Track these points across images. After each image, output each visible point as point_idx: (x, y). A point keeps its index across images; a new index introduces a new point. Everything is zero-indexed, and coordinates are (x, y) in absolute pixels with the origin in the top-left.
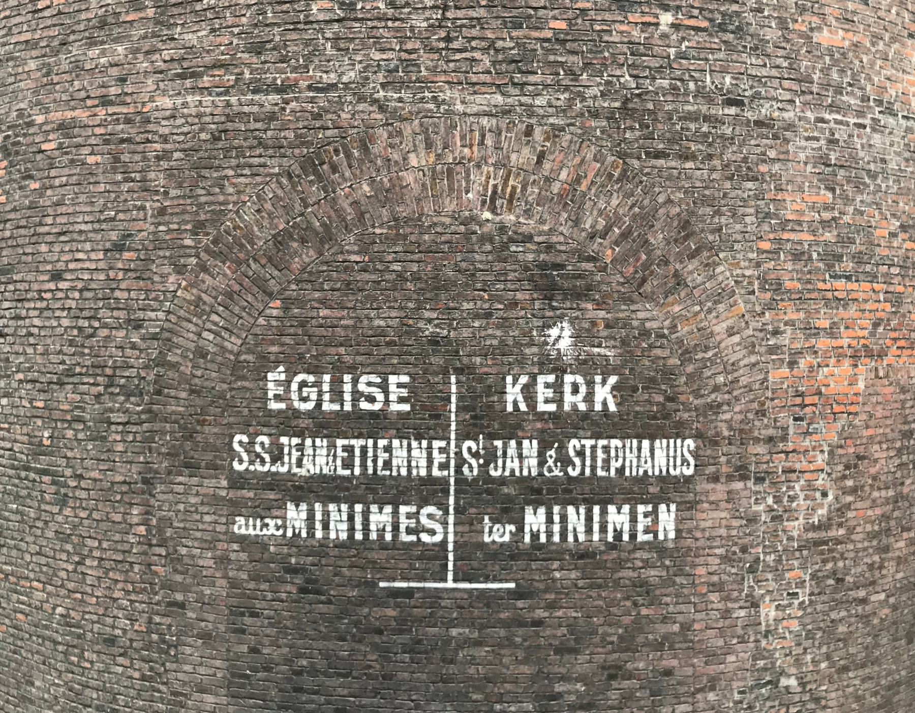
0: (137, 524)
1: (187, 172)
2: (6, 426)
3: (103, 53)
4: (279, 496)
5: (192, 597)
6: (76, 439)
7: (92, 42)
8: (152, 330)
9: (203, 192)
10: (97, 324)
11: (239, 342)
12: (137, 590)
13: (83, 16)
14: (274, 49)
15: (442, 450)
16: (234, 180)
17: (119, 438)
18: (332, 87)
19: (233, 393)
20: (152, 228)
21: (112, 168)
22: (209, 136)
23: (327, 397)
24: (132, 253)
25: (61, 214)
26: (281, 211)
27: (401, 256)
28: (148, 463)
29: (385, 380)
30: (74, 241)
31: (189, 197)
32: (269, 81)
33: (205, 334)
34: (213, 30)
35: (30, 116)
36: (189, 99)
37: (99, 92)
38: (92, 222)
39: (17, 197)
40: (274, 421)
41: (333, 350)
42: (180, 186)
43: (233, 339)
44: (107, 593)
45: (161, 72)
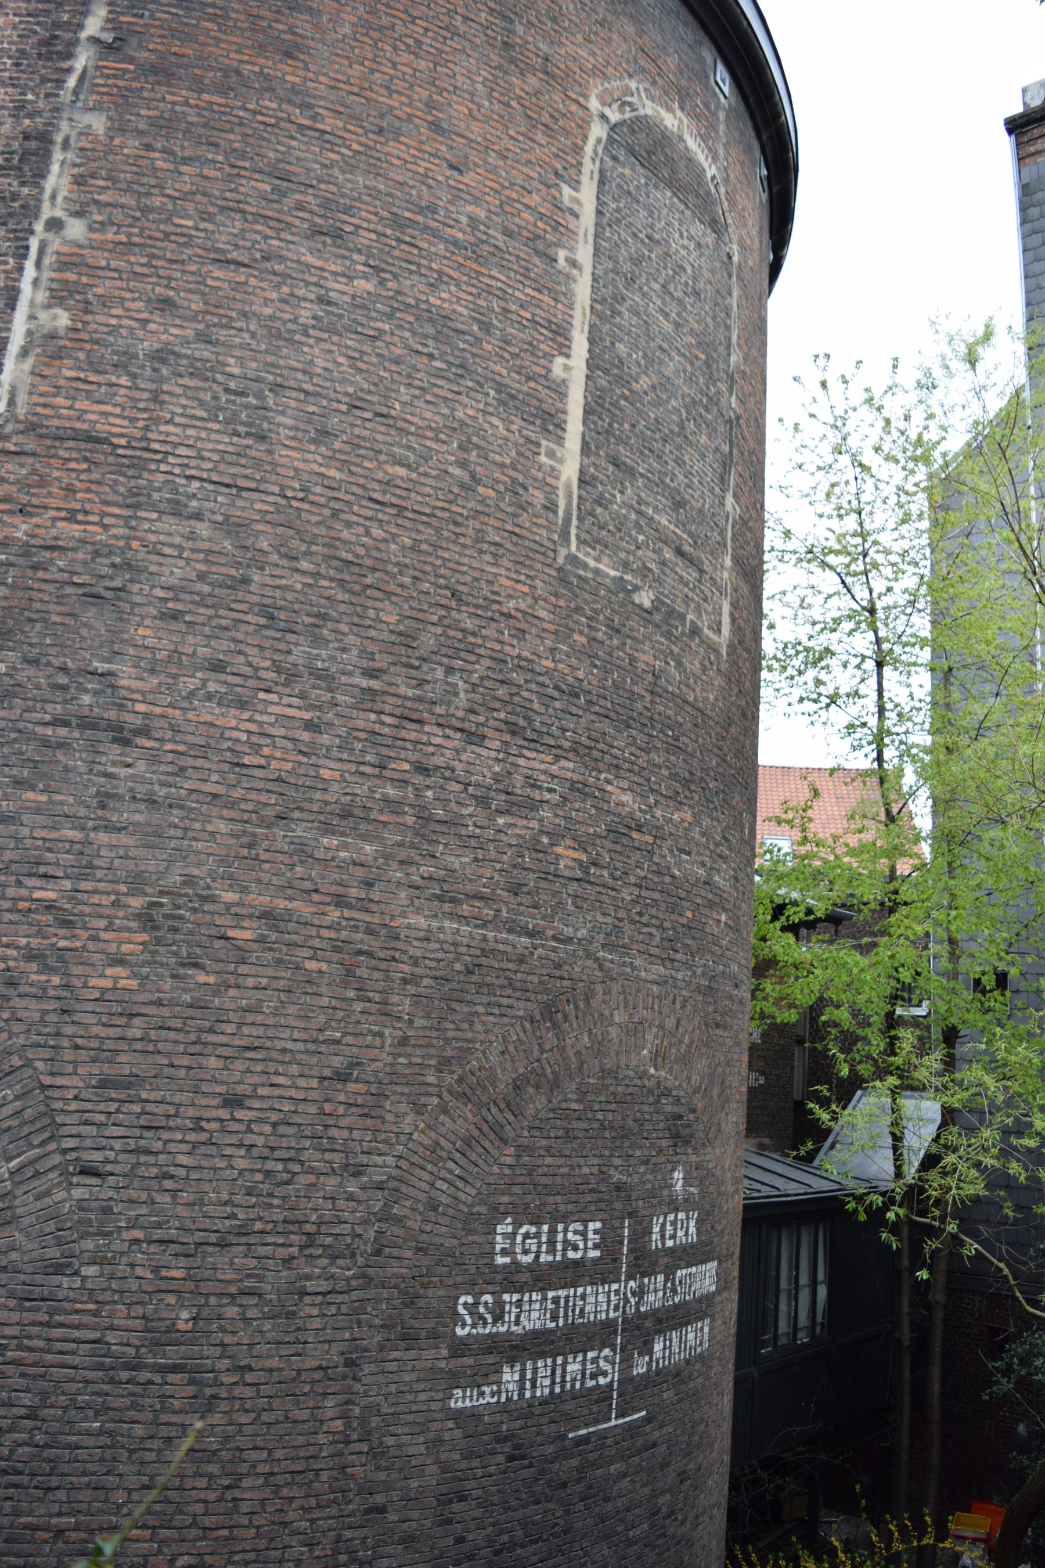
0: (332, 1419)
1: (436, 1002)
2: (91, 1306)
3: (344, 846)
4: (498, 1359)
5: (395, 1495)
6: (244, 1319)
7: (328, 829)
8: (377, 1178)
9: (452, 1026)
10: (297, 1168)
11: (474, 1192)
12: (324, 1503)
13: (318, 796)
14: (528, 893)
15: (617, 1292)
16: (484, 1018)
17: (315, 1311)
18: (569, 940)
19: (464, 1248)
20: (390, 1059)
21: (342, 981)
22: (463, 968)
23: (544, 1248)
24: (360, 1086)
25: (253, 1024)
26: (522, 1054)
27: (604, 1106)
28: (355, 1340)
29: (586, 1227)
30: (271, 1060)
31: (437, 1030)
32: (522, 924)
33: (439, 1184)
34: (476, 860)
35: (209, 888)
36: (447, 924)
37: (334, 889)
38: (305, 1041)
39: (167, 987)
40: (499, 1278)
41: (551, 1199)
42: (428, 1017)
43: (468, 1189)
44: (276, 1518)
45: (417, 888)
